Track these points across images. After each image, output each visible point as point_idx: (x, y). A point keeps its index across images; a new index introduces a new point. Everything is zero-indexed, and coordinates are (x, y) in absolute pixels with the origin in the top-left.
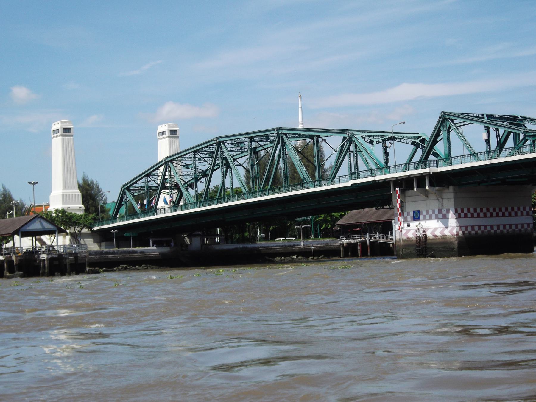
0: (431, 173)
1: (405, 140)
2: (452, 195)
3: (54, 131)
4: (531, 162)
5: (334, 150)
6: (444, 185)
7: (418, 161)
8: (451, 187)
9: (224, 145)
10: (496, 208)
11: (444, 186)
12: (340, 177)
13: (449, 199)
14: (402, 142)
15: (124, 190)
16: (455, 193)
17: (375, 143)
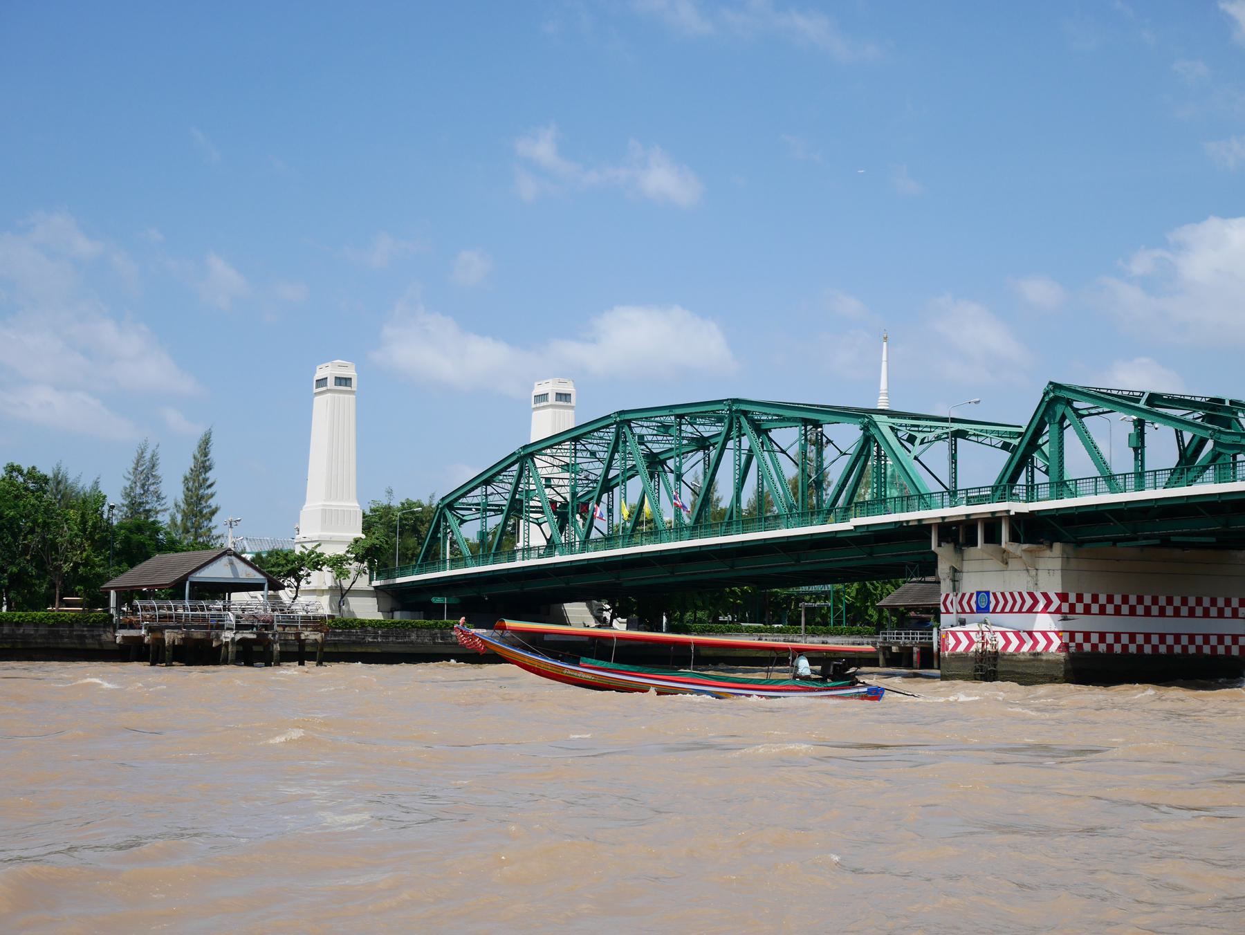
0: (1012, 513)
1: (989, 439)
2: (1057, 564)
3: (317, 381)
4: (1220, 501)
5: (841, 452)
6: (1041, 540)
7: (1174, 467)
8: (1057, 547)
9: (631, 428)
10: (1160, 597)
11: (1042, 543)
12: (1127, 476)
13: (1051, 572)
14: (980, 443)
15: (442, 509)
16: (1066, 558)
17: (918, 441)
